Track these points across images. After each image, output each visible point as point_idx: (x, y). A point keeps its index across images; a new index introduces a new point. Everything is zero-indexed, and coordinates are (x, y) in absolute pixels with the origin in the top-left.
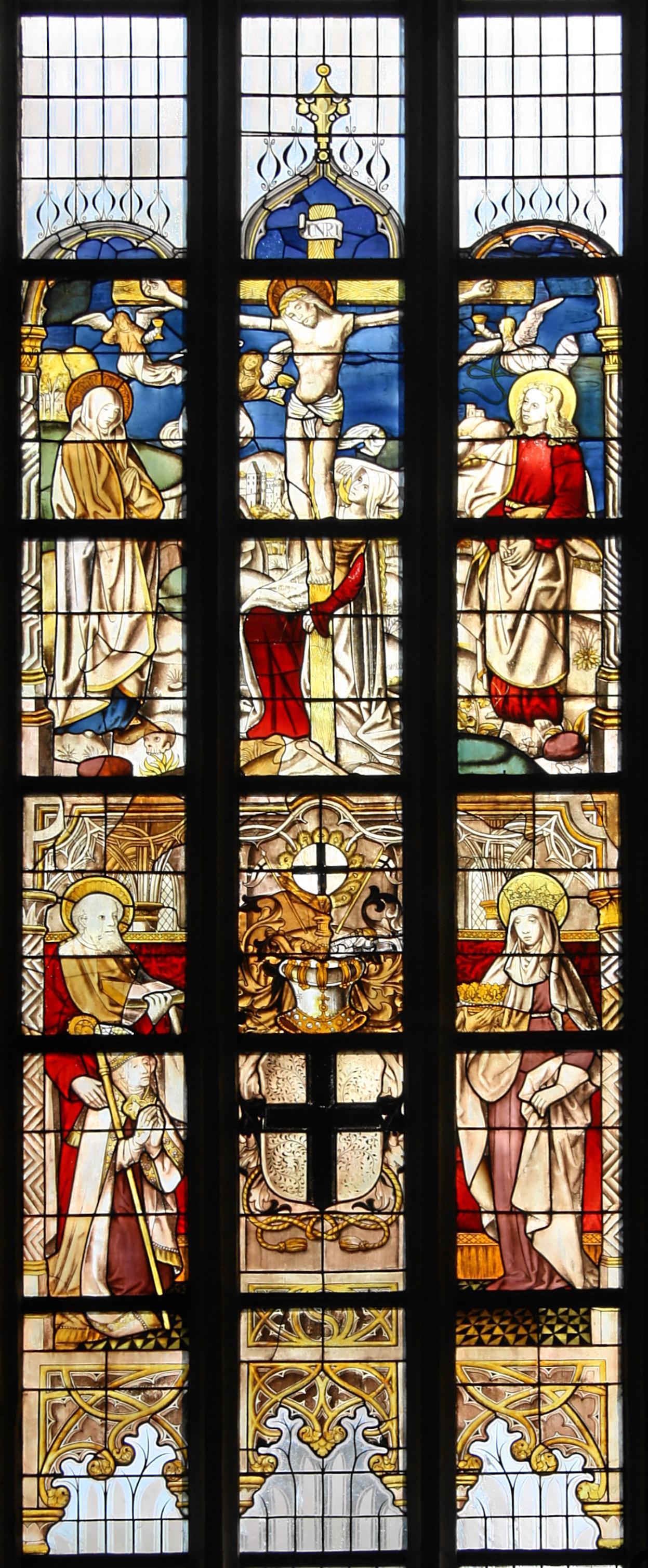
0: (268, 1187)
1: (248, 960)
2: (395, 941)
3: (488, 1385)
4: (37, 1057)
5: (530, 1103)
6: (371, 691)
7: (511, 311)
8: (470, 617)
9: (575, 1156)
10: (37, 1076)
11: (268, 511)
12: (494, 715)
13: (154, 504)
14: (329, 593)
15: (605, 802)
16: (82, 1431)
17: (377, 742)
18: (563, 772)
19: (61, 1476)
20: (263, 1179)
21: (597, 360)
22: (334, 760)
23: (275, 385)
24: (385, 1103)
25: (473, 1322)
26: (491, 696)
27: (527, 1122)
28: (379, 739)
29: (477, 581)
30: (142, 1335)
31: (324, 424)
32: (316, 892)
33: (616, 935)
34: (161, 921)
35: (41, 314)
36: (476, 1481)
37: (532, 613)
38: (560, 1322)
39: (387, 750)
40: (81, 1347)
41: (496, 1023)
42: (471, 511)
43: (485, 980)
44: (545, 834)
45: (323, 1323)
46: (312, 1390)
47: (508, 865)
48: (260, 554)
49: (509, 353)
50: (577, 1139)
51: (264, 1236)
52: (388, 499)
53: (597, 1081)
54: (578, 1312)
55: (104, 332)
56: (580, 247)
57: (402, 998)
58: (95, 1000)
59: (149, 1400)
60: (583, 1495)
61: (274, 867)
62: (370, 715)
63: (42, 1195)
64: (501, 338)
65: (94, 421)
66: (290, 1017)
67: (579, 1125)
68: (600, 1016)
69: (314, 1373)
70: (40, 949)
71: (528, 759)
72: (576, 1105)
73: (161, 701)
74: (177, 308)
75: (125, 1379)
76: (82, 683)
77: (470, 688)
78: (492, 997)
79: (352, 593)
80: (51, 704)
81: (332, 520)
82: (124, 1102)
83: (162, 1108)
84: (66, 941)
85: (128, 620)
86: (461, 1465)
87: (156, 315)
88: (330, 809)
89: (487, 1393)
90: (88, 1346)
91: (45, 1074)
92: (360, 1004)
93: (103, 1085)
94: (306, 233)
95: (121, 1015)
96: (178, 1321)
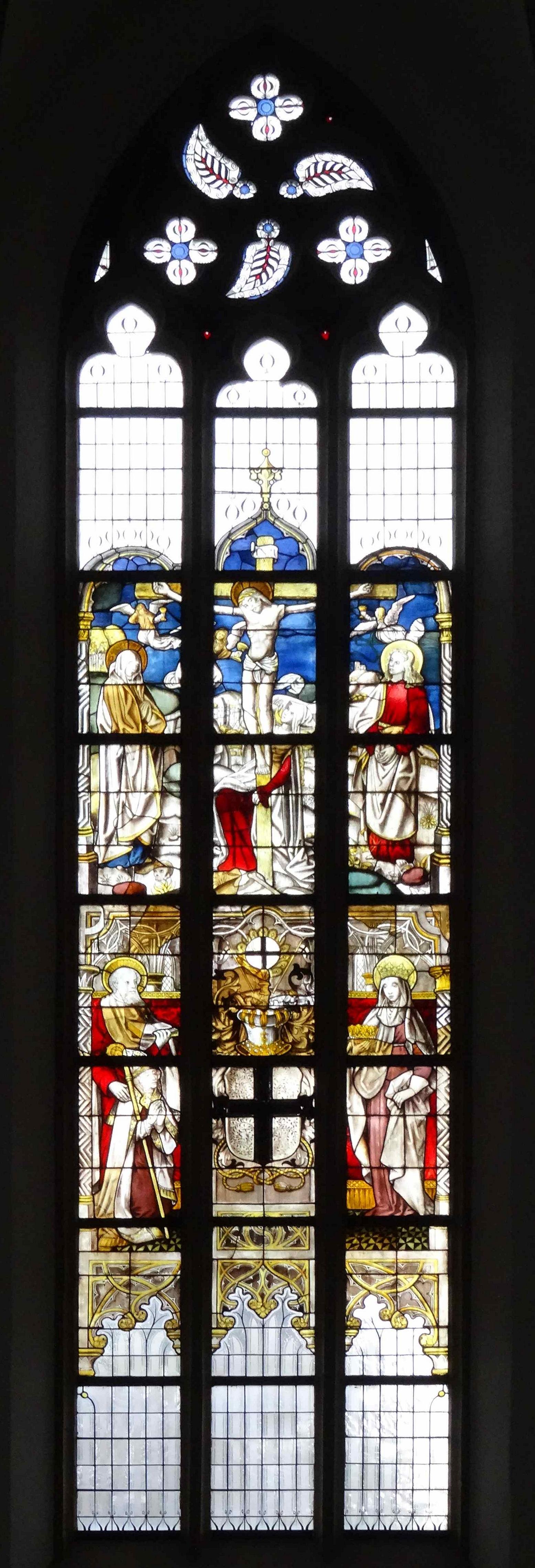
2: (309, 998)
3: (366, 1274)
5: (392, 1100)
6: (295, 841)
7: (382, 603)
9: (420, 1132)
19: (102, 1328)
20: (227, 1146)
21: (435, 635)
24: (303, 1099)
26: (369, 845)
27: (390, 1111)
29: (361, 773)
30: (152, 1242)
34: (164, 985)
35: (91, 605)
37: (395, 793)
38: (410, 1235)
40: (114, 1249)
43: (365, 1023)
46: (257, 1277)
47: (380, 951)
48: (226, 755)
49: (381, 630)
50: (421, 1122)
53: (434, 1086)
54: (421, 1229)
55: (129, 616)
57: (313, 1034)
59: (156, 1282)
67: (422, 1113)
68: (437, 1046)
69: (258, 1267)
70: (90, 1001)
71: (392, 884)
74: (175, 601)
79: (284, 780)
80: (96, 849)
83: (165, 1102)
88: (270, 916)
89: (365, 1279)
90: (119, 1249)
91: (92, 1079)
95: (139, 1044)
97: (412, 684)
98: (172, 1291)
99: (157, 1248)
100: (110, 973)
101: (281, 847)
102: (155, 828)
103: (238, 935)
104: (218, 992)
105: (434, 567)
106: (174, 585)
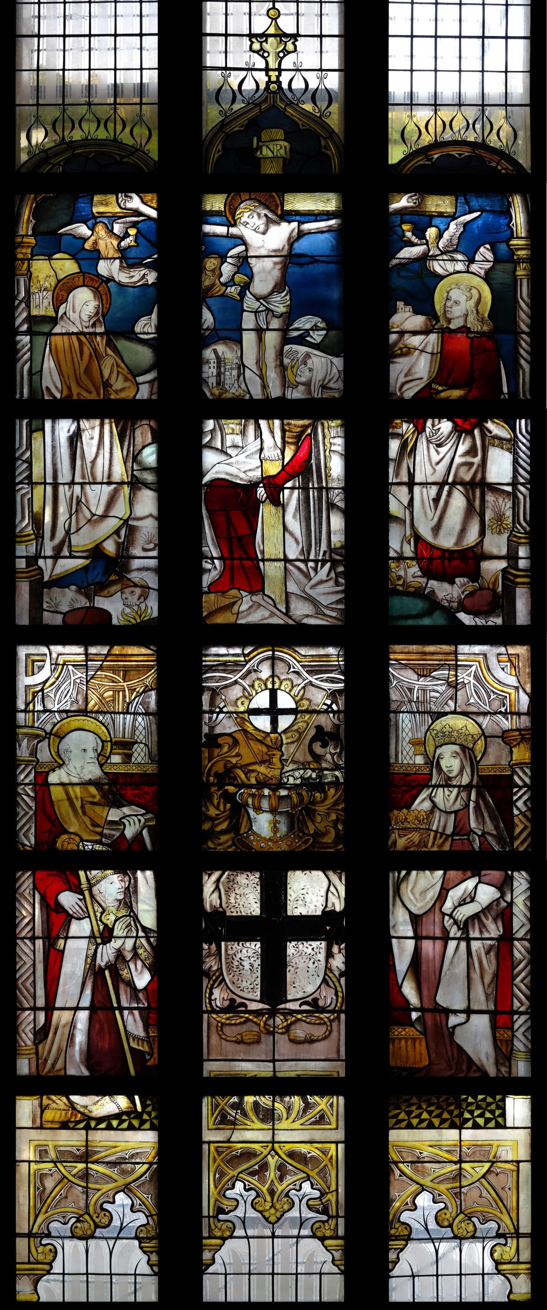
0: (228, 987)
1: (209, 789)
2: (337, 773)
3: (417, 1162)
4: (29, 873)
5: (451, 916)
6: (317, 554)
7: (436, 221)
8: (400, 488)
9: (489, 962)
10: (28, 891)
11: (226, 391)
12: (420, 573)
13: (129, 387)
14: (280, 468)
15: (518, 655)
16: (66, 1197)
17: (322, 597)
18: (479, 624)
19: (49, 1235)
20: (224, 980)
21: (509, 266)
22: (284, 611)
23: (232, 283)
24: (328, 915)
25: (403, 1108)
26: (417, 557)
27: (448, 933)
28: (324, 594)
29: (406, 457)
30: (118, 1116)
31: (274, 316)
32: (269, 730)
33: (528, 771)
34: (135, 755)
35: (31, 226)
36: (406, 1245)
37: (454, 484)
38: (479, 1107)
39: (331, 603)
40: (64, 1125)
41: (422, 844)
42: (402, 394)
43: (414, 807)
44: (466, 682)
45: (274, 1109)
46: (264, 1166)
47: (434, 708)
48: (219, 433)
49: (434, 258)
50: (491, 947)
51: (224, 1029)
52: (330, 381)
53: (508, 898)
54: (494, 1099)
55: (85, 240)
56: (494, 164)
57: (343, 823)
58: (78, 821)
59: (124, 1173)
60: (496, 1255)
61: (232, 709)
62: (317, 573)
63: (32, 990)
64: (427, 244)
65: (77, 315)
66: (246, 838)
67: (493, 935)
68: (513, 839)
69: (265, 1152)
70: (32, 776)
71: (450, 613)
72: (490, 918)
73: (136, 560)
74: (149, 218)
75: (103, 1154)
76: (67, 543)
77: (398, 550)
78: (419, 821)
79: (302, 469)
80: (41, 562)
81: (282, 399)
82: (102, 913)
83: (136, 918)
84: (54, 770)
85: (107, 489)
86: (393, 1232)
87: (130, 225)
88: (282, 660)
89: (416, 1171)
90: (71, 1125)
91: (35, 888)
92: (307, 828)
93: (84, 898)
94: (259, 153)
95: (101, 834)
96: (149, 1105)
97: (477, 332)
98: (147, 1186)
99: (125, 1125)
100: (61, 738)
101: (297, 560)
102: (123, 532)
103: (237, 686)
104: (211, 764)
105: (507, 169)
106: (148, 197)
